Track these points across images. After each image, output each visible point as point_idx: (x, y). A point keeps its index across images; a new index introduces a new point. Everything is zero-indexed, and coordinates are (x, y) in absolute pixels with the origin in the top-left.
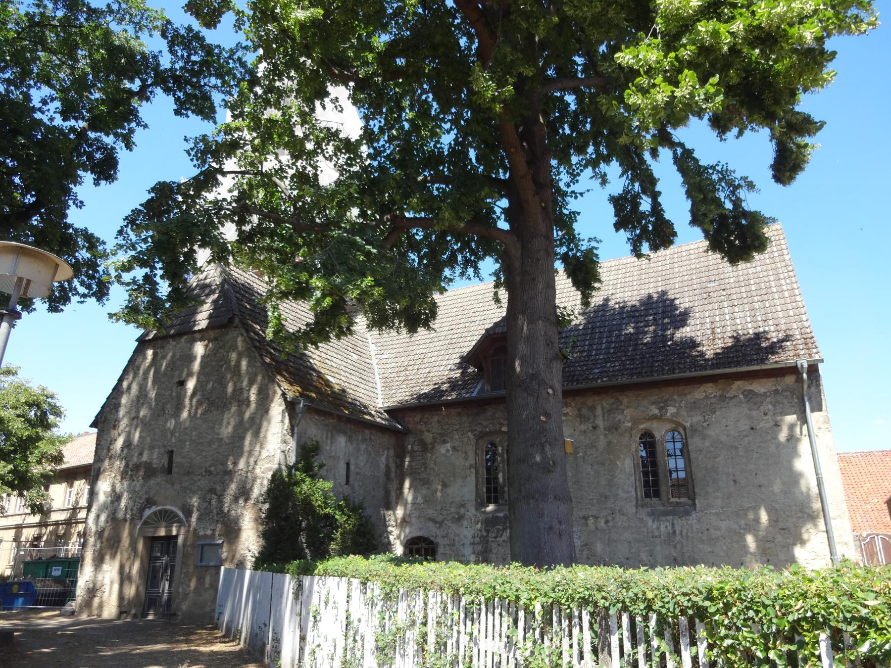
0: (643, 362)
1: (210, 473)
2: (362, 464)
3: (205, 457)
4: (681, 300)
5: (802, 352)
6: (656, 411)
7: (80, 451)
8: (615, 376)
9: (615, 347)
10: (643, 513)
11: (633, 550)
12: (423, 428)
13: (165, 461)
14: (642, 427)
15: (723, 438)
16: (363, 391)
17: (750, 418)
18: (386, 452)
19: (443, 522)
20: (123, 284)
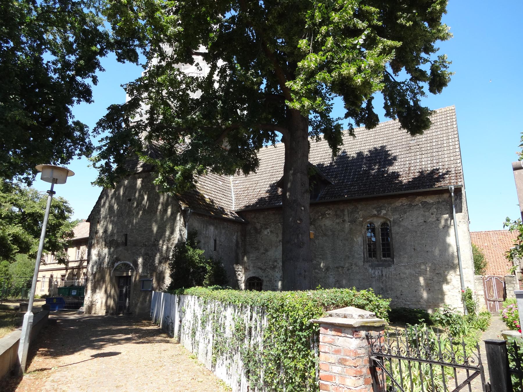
0: (370, 186)
1: (145, 245)
2: (223, 240)
3: (143, 237)
4: (393, 151)
5: (453, 181)
6: (376, 213)
7: (82, 231)
8: (354, 194)
9: (357, 177)
10: (367, 265)
11: (361, 284)
12: (256, 221)
13: (123, 239)
14: (368, 220)
15: (410, 227)
16: (224, 202)
17: (424, 216)
18: (236, 234)
19: (265, 269)
20: (96, 168)
